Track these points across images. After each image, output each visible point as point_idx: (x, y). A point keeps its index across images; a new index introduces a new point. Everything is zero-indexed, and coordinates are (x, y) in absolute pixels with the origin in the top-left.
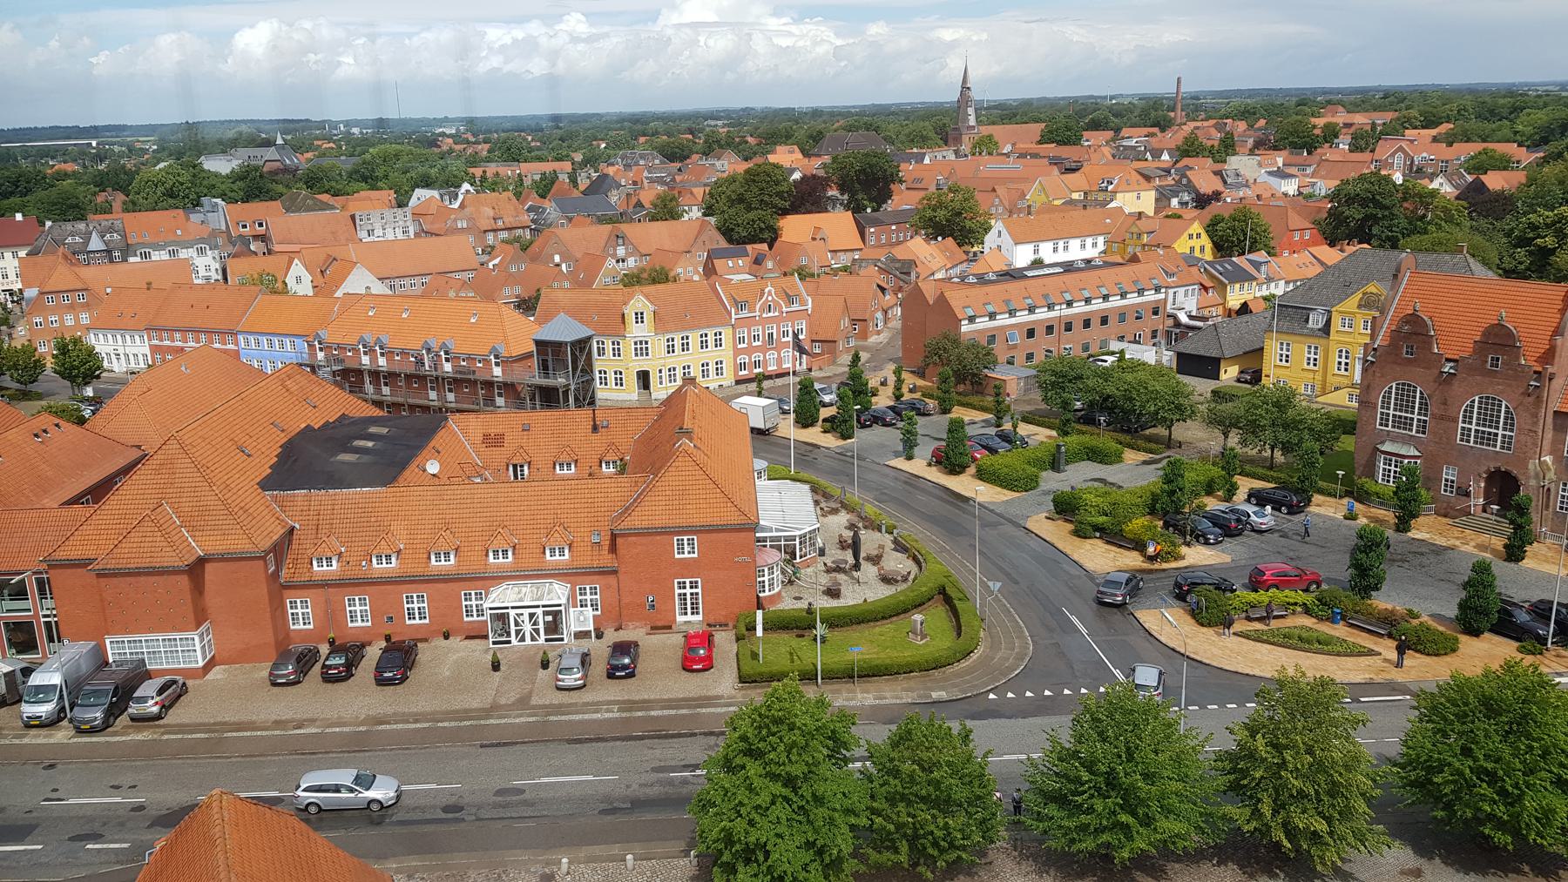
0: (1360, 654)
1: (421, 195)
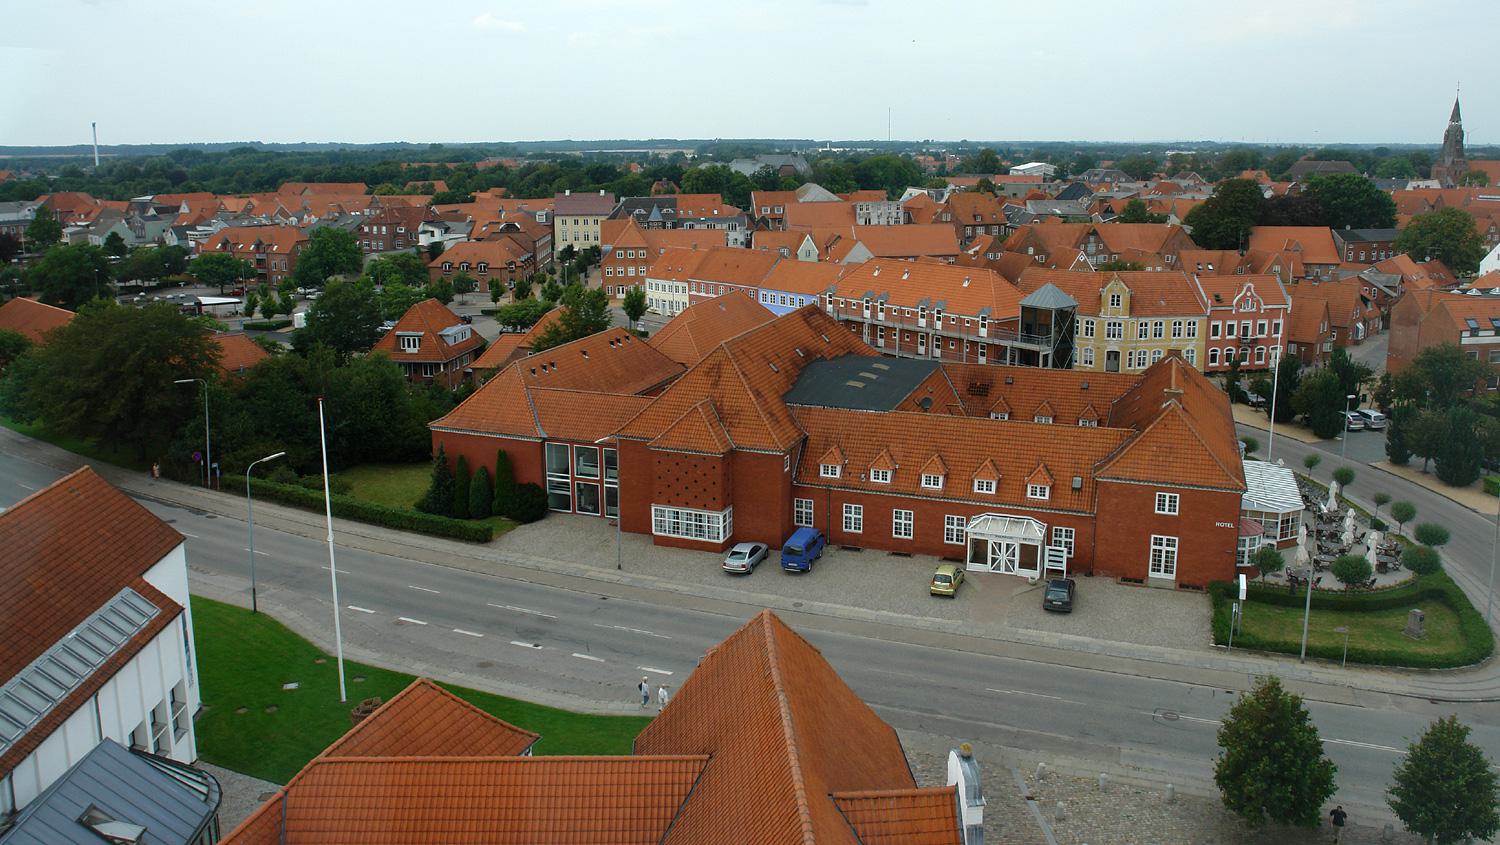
1: (912, 192)
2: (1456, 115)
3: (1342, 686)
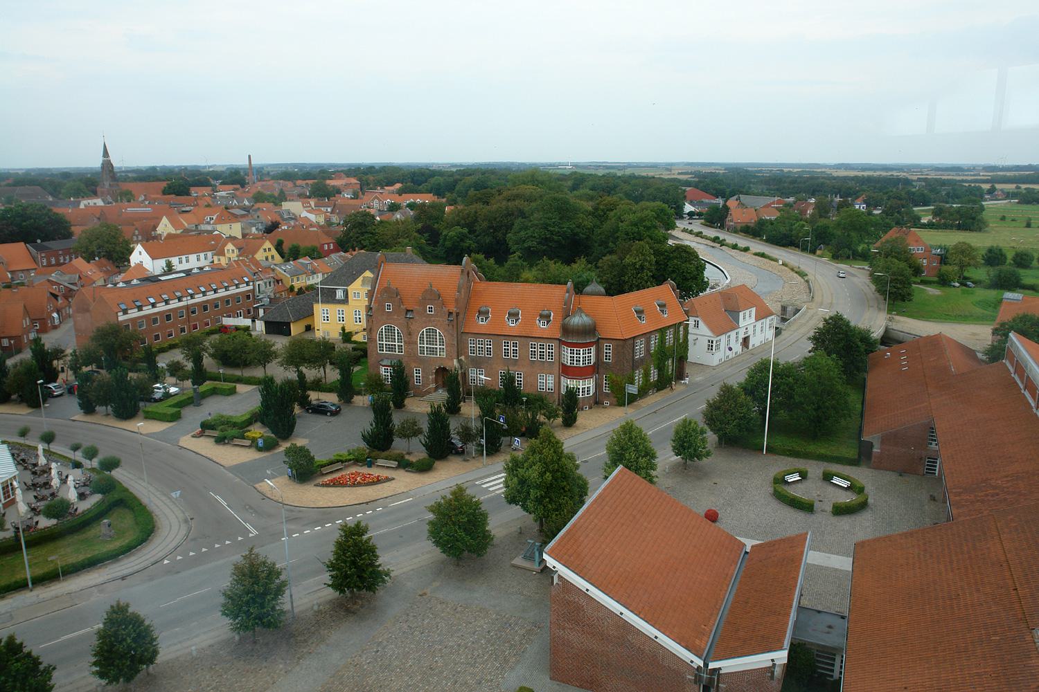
0: (373, 483)
2: (106, 153)
3: (63, 595)
